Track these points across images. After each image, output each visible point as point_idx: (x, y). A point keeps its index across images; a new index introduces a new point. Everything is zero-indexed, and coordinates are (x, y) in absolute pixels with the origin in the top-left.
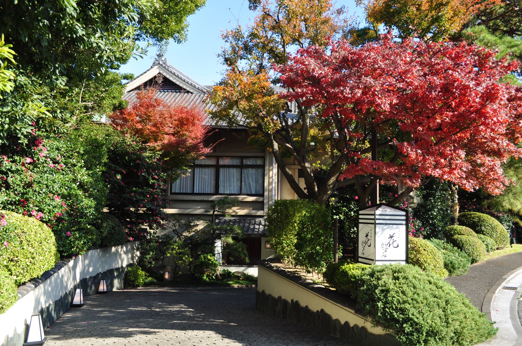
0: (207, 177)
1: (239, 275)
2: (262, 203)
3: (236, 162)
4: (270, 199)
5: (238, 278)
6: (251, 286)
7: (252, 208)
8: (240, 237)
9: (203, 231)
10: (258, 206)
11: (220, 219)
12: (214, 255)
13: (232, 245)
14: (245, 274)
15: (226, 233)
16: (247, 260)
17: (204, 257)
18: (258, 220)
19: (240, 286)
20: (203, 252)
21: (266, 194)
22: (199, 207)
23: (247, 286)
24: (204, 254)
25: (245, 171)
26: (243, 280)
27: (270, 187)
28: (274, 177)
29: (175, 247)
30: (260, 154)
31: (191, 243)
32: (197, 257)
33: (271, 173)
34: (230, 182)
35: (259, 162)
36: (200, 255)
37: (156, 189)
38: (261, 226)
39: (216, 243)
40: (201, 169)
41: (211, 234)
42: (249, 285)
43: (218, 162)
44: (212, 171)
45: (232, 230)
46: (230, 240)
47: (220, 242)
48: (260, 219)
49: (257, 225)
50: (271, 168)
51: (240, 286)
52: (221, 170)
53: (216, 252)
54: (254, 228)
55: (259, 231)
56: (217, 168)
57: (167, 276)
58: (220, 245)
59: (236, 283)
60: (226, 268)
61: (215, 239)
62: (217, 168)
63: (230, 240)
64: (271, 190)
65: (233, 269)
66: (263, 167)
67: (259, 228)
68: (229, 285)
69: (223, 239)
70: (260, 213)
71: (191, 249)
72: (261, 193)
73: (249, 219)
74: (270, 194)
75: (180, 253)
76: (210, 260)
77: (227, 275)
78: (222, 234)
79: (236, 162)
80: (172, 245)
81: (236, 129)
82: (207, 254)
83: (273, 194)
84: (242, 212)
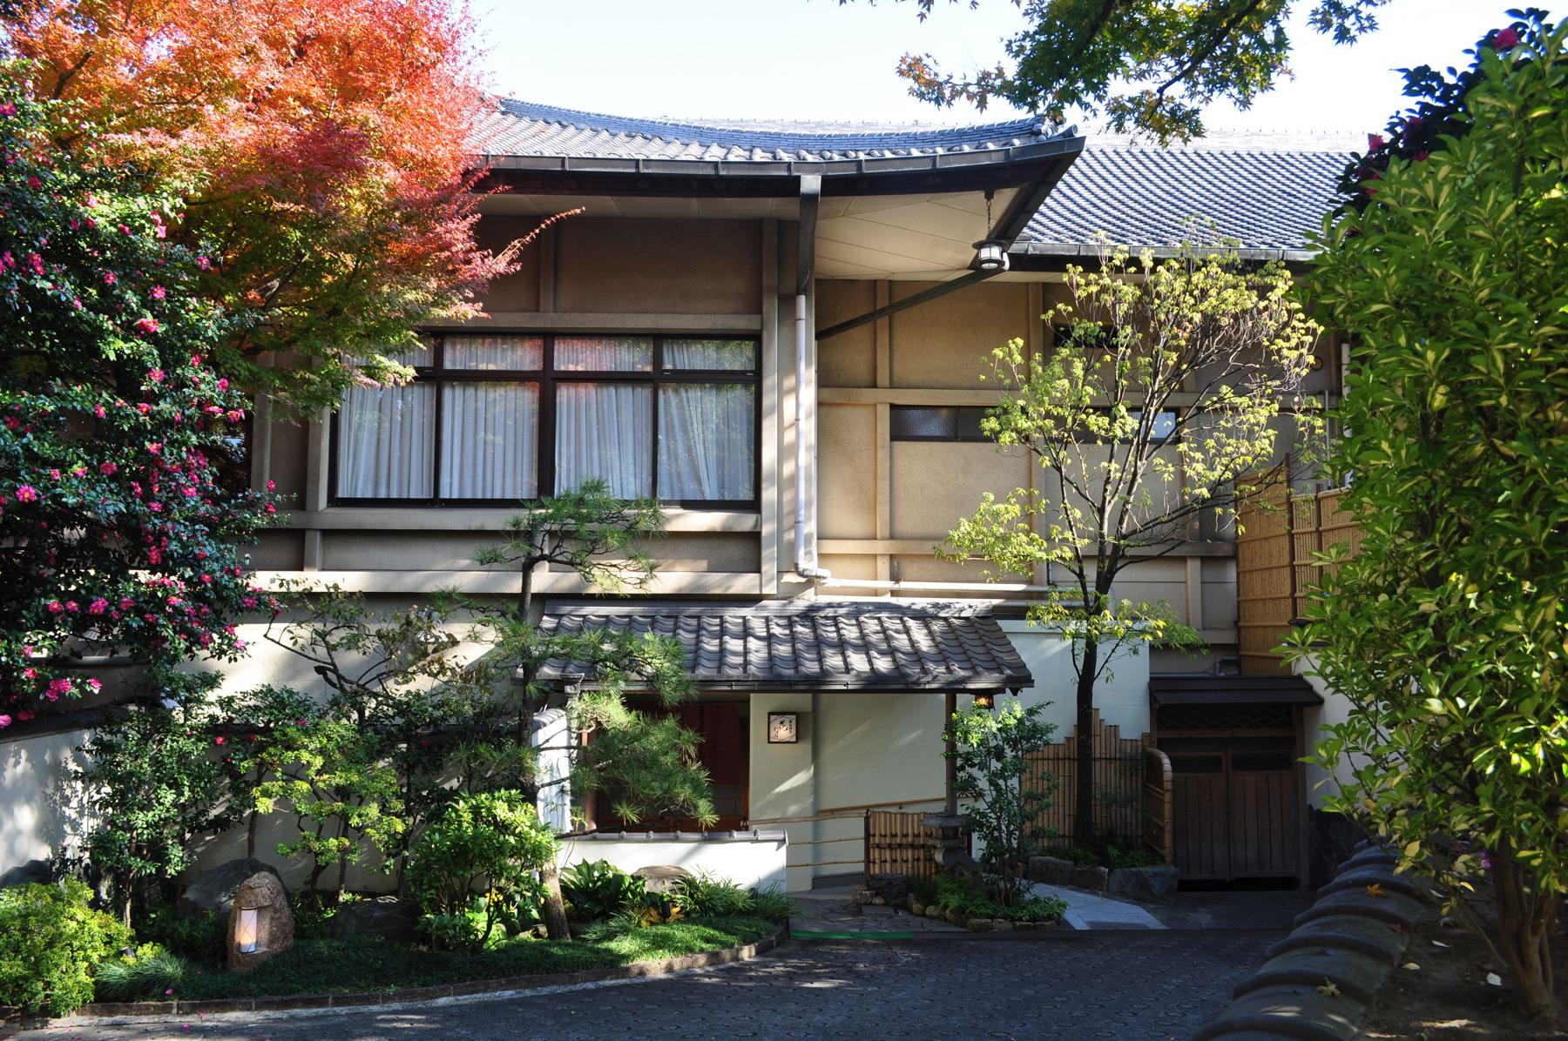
0: (499, 440)
1: (664, 889)
2: (754, 537)
3: (632, 358)
4: (787, 522)
5: (658, 907)
6: (736, 958)
7: (704, 564)
8: (669, 693)
9: (478, 673)
10: (735, 551)
11: (560, 616)
12: (530, 795)
13: (625, 737)
14: (691, 883)
15: (594, 670)
16: (706, 812)
17: (475, 811)
18: (733, 615)
19: (679, 962)
20: (479, 782)
21: (769, 494)
22: (465, 562)
23: (714, 958)
24: (474, 792)
25: (670, 399)
26: (687, 917)
27: (788, 468)
28: (803, 425)
29: (305, 756)
30: (741, 323)
31: (406, 733)
32: (435, 806)
33: (789, 404)
34: (603, 446)
35: (734, 358)
36: (453, 794)
37: (153, 398)
38: (753, 644)
39: (539, 726)
40: (470, 391)
41: (514, 680)
42: (726, 954)
43: (548, 358)
44: (525, 399)
45: (625, 661)
46: (616, 714)
47: (563, 723)
48: (747, 612)
49: (734, 637)
50: (789, 382)
51: (679, 962)
52: (564, 394)
53: (542, 778)
54: (723, 651)
55: (746, 663)
56: (547, 381)
57: (249, 933)
58: (562, 740)
59: (660, 943)
60: (592, 853)
61: (537, 707)
62: (547, 381)
63: (616, 714)
64: (793, 481)
65: (630, 857)
66: (753, 379)
67: (746, 652)
68: (614, 963)
69: (575, 704)
70: (743, 584)
71: (406, 766)
72: (746, 494)
73: (694, 610)
74: (787, 497)
75: (343, 793)
76: (503, 827)
77: (600, 898)
78: (572, 682)
79: (632, 358)
80: (290, 746)
81: (638, 173)
82: (491, 788)
83: (802, 496)
84: (671, 579)
